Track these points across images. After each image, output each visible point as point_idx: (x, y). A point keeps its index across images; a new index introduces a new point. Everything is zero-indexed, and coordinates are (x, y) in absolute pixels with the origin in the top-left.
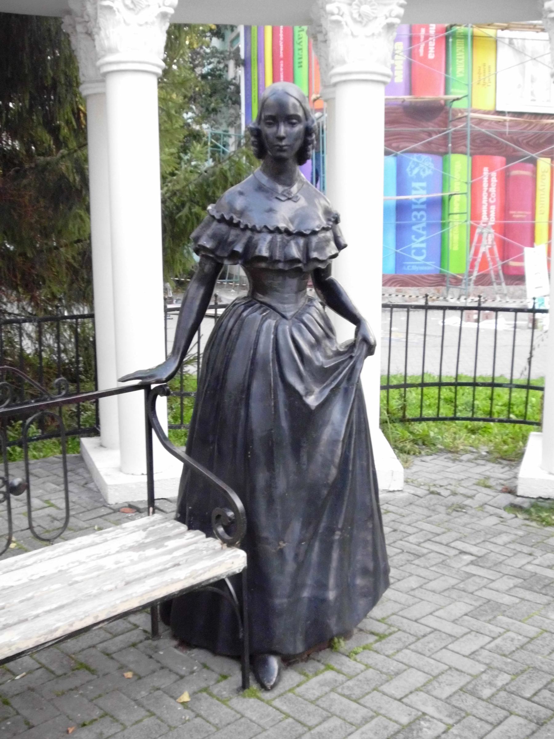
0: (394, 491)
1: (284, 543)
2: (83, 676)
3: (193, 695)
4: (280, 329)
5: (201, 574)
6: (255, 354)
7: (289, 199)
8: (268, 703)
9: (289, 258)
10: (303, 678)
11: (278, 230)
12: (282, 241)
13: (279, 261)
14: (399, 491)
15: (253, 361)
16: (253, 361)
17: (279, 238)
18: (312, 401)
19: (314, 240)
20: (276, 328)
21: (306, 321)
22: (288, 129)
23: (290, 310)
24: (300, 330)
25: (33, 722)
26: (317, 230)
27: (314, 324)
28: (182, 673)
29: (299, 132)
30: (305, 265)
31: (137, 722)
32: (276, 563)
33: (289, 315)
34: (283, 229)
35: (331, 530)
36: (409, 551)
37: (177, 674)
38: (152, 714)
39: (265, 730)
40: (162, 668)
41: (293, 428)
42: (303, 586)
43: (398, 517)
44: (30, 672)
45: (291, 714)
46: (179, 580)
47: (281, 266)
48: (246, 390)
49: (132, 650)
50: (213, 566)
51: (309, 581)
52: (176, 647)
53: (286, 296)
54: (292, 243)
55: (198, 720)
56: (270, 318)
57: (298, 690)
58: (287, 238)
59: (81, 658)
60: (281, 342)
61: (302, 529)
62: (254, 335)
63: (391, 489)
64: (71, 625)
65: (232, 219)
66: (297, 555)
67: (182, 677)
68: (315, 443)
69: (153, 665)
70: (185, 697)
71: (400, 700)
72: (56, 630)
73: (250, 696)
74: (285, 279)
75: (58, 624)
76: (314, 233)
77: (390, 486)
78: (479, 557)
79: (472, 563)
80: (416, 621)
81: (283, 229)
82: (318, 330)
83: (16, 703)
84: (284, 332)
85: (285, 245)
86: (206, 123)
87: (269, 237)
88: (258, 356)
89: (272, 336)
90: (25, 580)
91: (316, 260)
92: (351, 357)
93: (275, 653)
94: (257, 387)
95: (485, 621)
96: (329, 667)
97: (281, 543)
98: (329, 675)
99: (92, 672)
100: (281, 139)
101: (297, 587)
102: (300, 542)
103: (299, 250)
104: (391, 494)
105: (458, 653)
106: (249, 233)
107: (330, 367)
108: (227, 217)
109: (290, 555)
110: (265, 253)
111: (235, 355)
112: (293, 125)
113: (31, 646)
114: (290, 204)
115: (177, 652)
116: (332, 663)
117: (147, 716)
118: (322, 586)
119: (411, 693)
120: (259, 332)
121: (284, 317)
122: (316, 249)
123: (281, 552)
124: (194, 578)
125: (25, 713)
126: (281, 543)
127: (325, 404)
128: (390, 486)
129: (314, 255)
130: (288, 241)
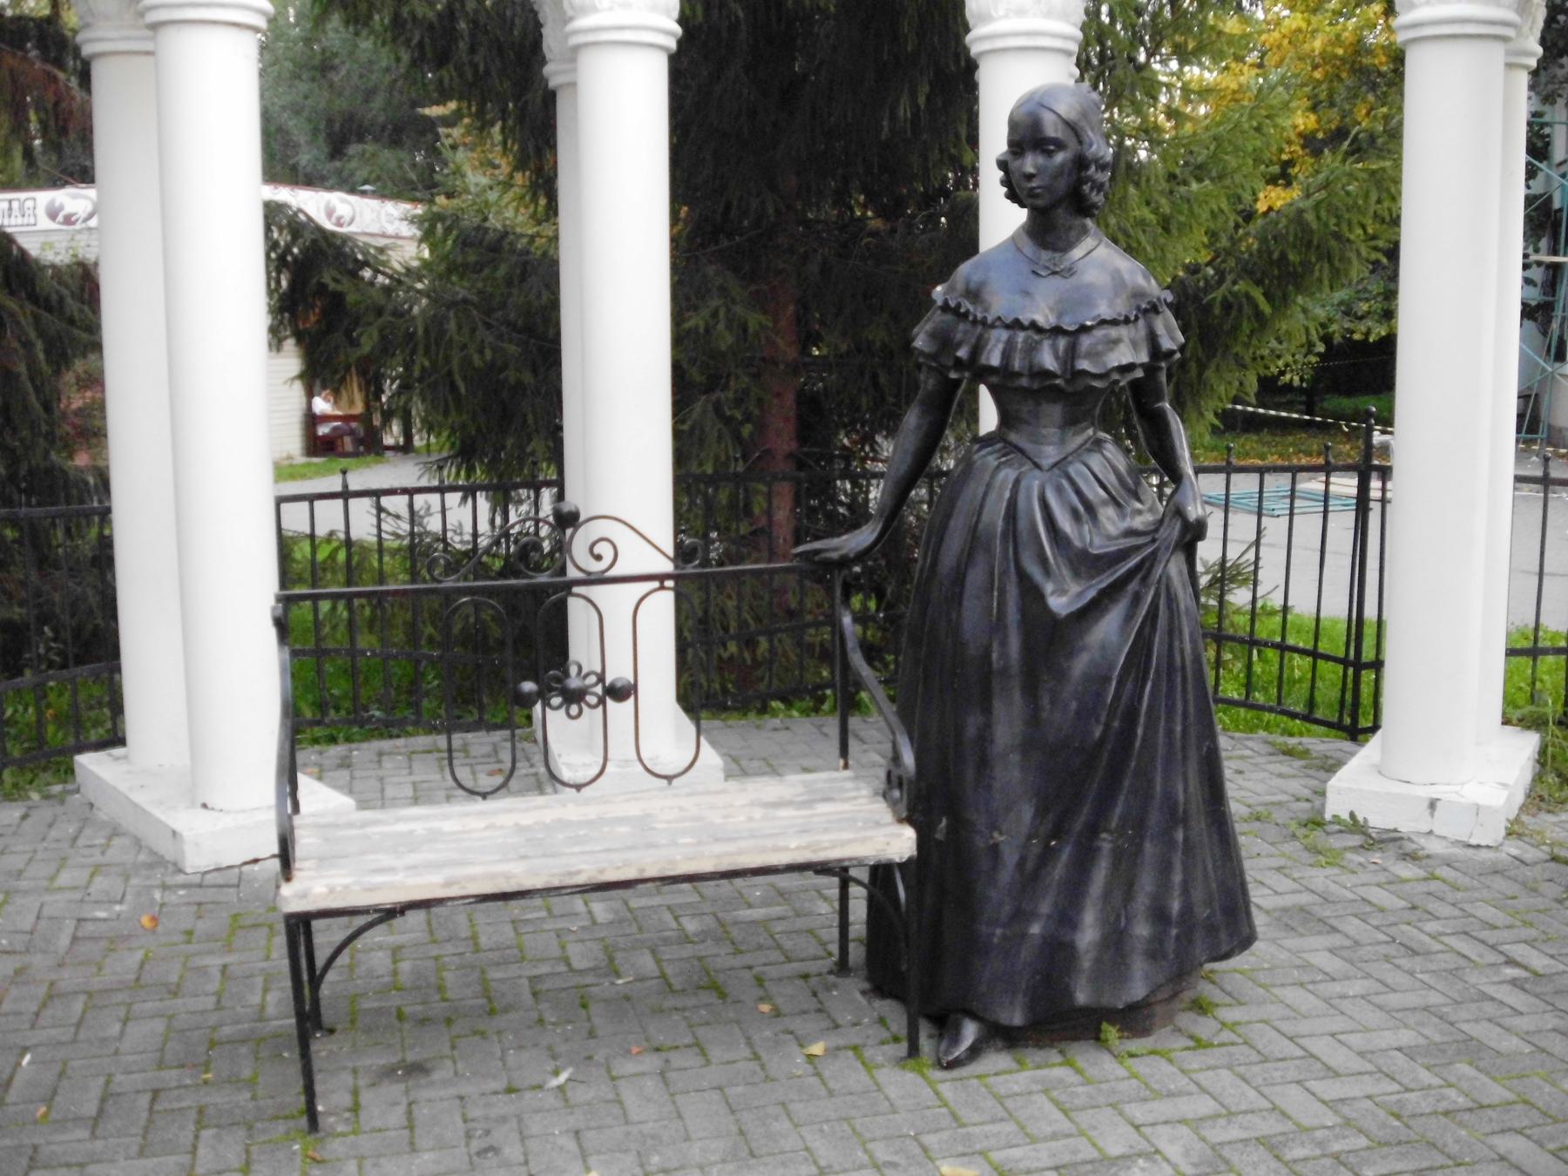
0: (1478, 846)
1: (1001, 834)
2: (711, 998)
3: (832, 1052)
4: (1023, 484)
5: (826, 849)
6: (977, 522)
7: (1054, 273)
8: (931, 1083)
9: (1036, 369)
10: (1014, 1065)
11: (1034, 326)
12: (1025, 341)
13: (1019, 375)
14: (1488, 847)
15: (974, 529)
16: (974, 529)
17: (1021, 336)
18: (1060, 603)
19: (1086, 342)
20: (1017, 482)
21: (1073, 475)
22: (1041, 160)
23: (1050, 454)
24: (1059, 490)
25: (600, 1033)
26: (1089, 323)
27: (1086, 480)
28: (840, 1022)
29: (1062, 165)
30: (1067, 381)
31: (728, 1063)
32: (984, 864)
33: (1046, 463)
34: (1026, 323)
35: (1093, 830)
36: (1405, 941)
37: (833, 1021)
38: (756, 1057)
39: (895, 1112)
40: (819, 1011)
41: (1028, 648)
42: (1032, 916)
43: (1446, 888)
44: (642, 979)
45: (951, 1104)
46: (786, 849)
47: (1024, 382)
48: (959, 578)
49: (800, 982)
50: (850, 841)
51: (1045, 907)
52: (863, 993)
53: (1044, 431)
54: (1046, 344)
55: (814, 1080)
56: (1011, 466)
57: (992, 1080)
58: (1036, 337)
59: (721, 978)
60: (1021, 503)
61: (1035, 817)
62: (981, 490)
63: (1474, 842)
64: (601, 872)
65: (959, 305)
66: (1023, 860)
67: (837, 1026)
68: (1061, 675)
69: (812, 1004)
70: (817, 1049)
71: (1137, 1127)
72: (578, 872)
73: (913, 1070)
74: (1038, 404)
75: (583, 867)
76: (1084, 329)
77: (1471, 835)
78: (1536, 974)
79: (1514, 982)
80: (1291, 1039)
81: (1026, 323)
82: (1096, 494)
83: (595, 1009)
84: (1029, 490)
85: (1031, 348)
86: (1206, 116)
87: (1004, 335)
88: (981, 527)
89: (1007, 495)
90: (593, 817)
91: (1084, 373)
92: (1154, 541)
93: (974, 1016)
94: (975, 577)
95: (1422, 1065)
96: (1069, 1063)
97: (996, 835)
98: (1060, 1072)
99: (722, 995)
100: (1030, 177)
101: (1021, 916)
102: (1030, 837)
103: (1057, 357)
104: (1471, 852)
105: (1313, 1094)
106: (979, 329)
107: (1106, 554)
108: (952, 304)
109: (1010, 857)
110: (995, 360)
111: (952, 523)
112: (1049, 154)
113: (539, 886)
114: (1056, 281)
115: (859, 997)
116: (1080, 1062)
117: (747, 1059)
118: (1067, 918)
119: (1166, 1122)
120: (989, 486)
121: (1037, 466)
122: (1090, 355)
123: (995, 850)
124: (814, 851)
125: (597, 1021)
126: (996, 835)
127: (1089, 613)
128: (1471, 835)
129: (1084, 365)
130: (1039, 343)
